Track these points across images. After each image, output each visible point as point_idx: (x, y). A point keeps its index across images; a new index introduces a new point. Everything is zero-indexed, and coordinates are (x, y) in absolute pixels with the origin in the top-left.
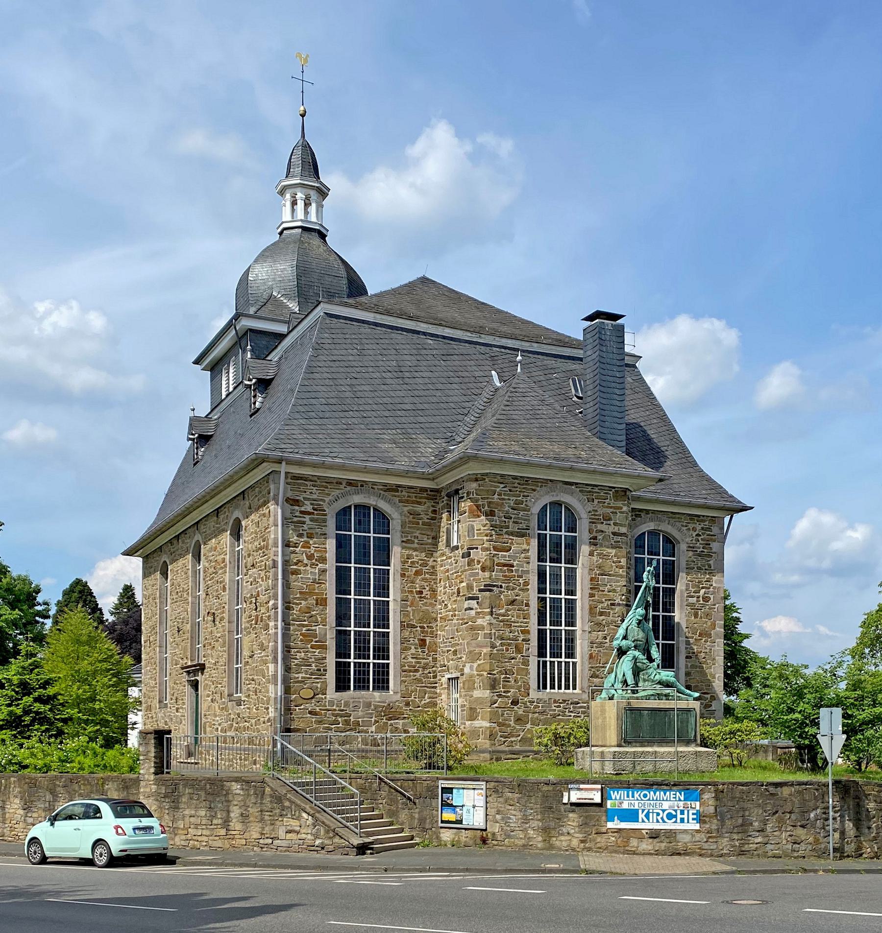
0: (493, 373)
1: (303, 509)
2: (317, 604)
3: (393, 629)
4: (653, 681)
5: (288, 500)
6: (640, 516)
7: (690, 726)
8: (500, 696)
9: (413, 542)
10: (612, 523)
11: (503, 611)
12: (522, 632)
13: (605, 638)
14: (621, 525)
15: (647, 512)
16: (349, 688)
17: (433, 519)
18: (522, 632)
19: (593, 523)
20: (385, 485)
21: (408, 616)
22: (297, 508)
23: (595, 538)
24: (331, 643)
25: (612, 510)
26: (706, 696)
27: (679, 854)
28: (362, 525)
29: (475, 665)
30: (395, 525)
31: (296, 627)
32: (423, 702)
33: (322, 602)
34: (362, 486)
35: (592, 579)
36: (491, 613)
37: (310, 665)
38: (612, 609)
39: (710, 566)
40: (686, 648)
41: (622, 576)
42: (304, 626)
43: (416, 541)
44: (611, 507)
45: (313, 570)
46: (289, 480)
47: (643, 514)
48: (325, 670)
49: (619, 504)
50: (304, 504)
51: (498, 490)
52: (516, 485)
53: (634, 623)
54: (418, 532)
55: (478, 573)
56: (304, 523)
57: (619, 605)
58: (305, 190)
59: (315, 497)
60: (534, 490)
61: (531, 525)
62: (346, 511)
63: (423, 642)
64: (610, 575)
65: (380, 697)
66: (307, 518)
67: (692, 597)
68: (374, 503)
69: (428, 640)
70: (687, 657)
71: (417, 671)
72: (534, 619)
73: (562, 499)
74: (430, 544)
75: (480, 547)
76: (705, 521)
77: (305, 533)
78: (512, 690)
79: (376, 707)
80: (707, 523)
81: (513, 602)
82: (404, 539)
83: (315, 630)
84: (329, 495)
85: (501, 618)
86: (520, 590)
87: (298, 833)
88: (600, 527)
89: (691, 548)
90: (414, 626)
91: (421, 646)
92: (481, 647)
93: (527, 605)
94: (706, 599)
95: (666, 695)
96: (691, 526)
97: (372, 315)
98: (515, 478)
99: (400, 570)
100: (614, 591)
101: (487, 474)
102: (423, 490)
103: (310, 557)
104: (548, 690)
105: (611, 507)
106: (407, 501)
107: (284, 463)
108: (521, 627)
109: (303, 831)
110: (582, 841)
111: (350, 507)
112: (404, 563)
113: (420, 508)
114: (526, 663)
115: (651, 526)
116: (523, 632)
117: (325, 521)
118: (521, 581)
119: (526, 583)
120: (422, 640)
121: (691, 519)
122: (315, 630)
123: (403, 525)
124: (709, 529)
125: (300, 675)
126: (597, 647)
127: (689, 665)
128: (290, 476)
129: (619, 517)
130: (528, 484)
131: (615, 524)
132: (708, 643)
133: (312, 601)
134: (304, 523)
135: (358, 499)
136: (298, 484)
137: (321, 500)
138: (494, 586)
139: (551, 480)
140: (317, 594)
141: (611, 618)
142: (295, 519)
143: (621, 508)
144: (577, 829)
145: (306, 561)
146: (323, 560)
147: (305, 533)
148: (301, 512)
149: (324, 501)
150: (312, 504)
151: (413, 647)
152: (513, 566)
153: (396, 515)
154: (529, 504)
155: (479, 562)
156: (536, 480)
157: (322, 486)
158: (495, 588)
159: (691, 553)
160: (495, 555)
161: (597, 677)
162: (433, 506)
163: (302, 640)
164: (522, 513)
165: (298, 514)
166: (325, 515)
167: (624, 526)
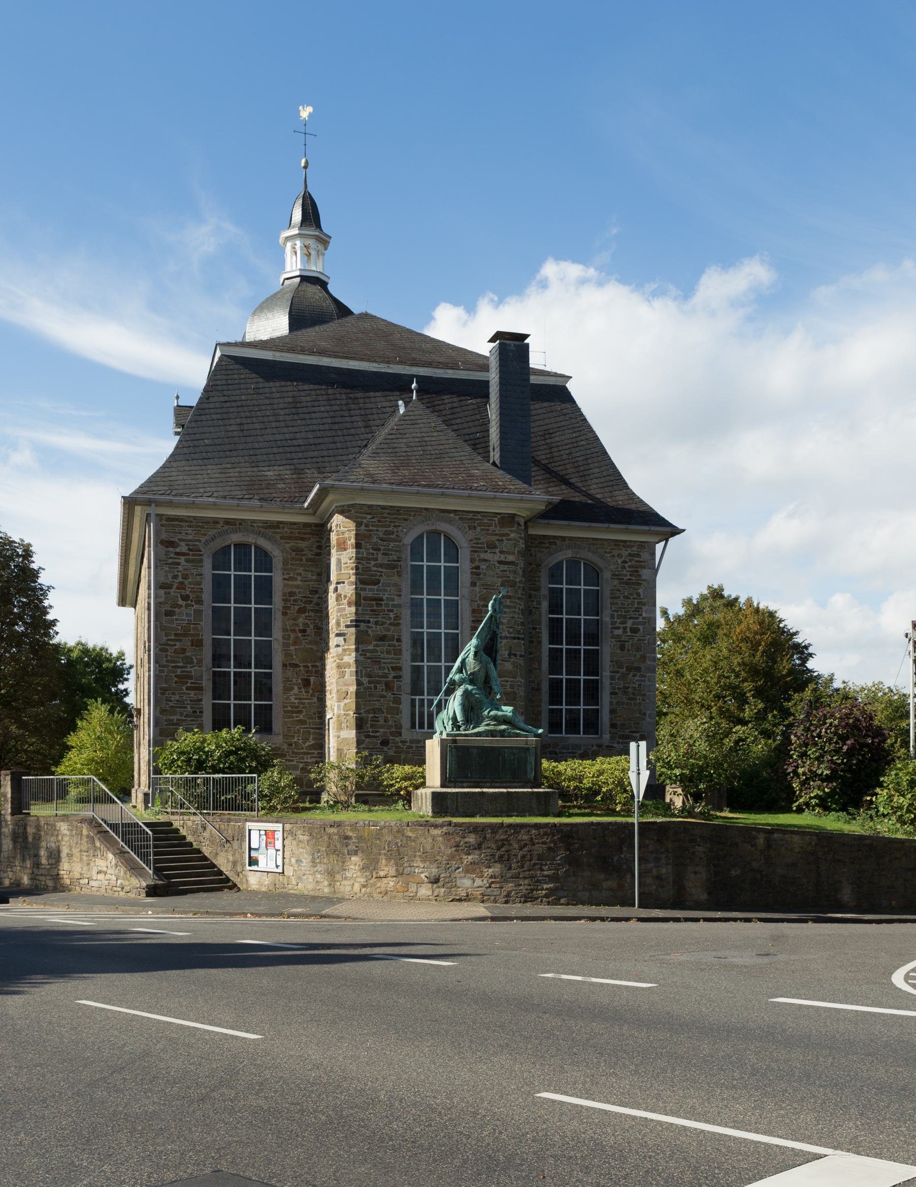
0: (400, 402)
1: (178, 550)
2: (192, 645)
3: (277, 671)
5: (162, 542)
6: (555, 543)
7: (529, 767)
8: (368, 736)
9: (296, 579)
10: (497, 551)
11: (371, 647)
12: (393, 668)
14: (508, 553)
15: (563, 539)
17: (318, 554)
18: (393, 668)
19: (475, 552)
20: (266, 522)
22: (171, 549)
23: (478, 568)
25: (496, 537)
26: (635, 735)
27: (460, 900)
28: (243, 564)
29: (342, 704)
30: (277, 563)
32: (307, 744)
33: (198, 643)
34: (240, 524)
35: (474, 611)
39: (639, 594)
40: (611, 684)
43: (299, 578)
44: (497, 535)
46: (164, 522)
47: (558, 542)
48: (201, 712)
49: (506, 530)
50: (178, 545)
51: (365, 521)
52: (385, 515)
53: (472, 653)
54: (302, 569)
55: (344, 609)
56: (179, 564)
57: (506, 638)
58: (304, 240)
59: (190, 537)
60: (406, 520)
62: (225, 550)
63: (306, 683)
67: (618, 628)
68: (254, 541)
69: (312, 679)
70: (612, 693)
71: (300, 712)
72: (407, 654)
73: (439, 528)
74: (314, 581)
75: (346, 581)
76: (632, 547)
77: (180, 574)
78: (382, 730)
80: (635, 549)
81: (382, 638)
82: (286, 577)
83: (191, 672)
85: (368, 655)
86: (391, 624)
87: (106, 873)
88: (483, 556)
89: (614, 576)
90: (296, 666)
91: (305, 686)
92: (347, 685)
93: (399, 640)
94: (634, 630)
96: (616, 552)
97: (271, 353)
98: (384, 508)
99: (281, 608)
101: (352, 505)
102: (306, 525)
103: (185, 598)
104: (426, 729)
105: (497, 535)
106: (289, 538)
107: (153, 505)
108: (391, 663)
109: (109, 872)
110: (364, 886)
111: (229, 546)
112: (285, 600)
113: (302, 544)
114: (398, 701)
115: (569, 554)
116: (393, 669)
117: (201, 561)
118: (392, 615)
119: (397, 617)
120: (306, 680)
121: (615, 545)
123: (285, 562)
124: (638, 555)
127: (615, 701)
128: (164, 518)
129: (506, 545)
130: (400, 514)
131: (502, 552)
132: (637, 678)
133: (187, 641)
134: (179, 564)
135: (236, 538)
136: (173, 526)
137: (197, 540)
139: (426, 509)
142: (170, 561)
143: (509, 535)
144: (359, 873)
145: (181, 602)
146: (199, 601)
147: (180, 574)
148: (176, 553)
149: (200, 541)
150: (187, 545)
151: (296, 688)
152: (382, 600)
153: (277, 554)
154: (400, 534)
155: (345, 597)
156: (408, 510)
157: (198, 526)
159: (616, 582)
162: (318, 542)
163: (176, 682)
164: (392, 544)
165: (172, 555)
166: (202, 555)
167: (513, 554)
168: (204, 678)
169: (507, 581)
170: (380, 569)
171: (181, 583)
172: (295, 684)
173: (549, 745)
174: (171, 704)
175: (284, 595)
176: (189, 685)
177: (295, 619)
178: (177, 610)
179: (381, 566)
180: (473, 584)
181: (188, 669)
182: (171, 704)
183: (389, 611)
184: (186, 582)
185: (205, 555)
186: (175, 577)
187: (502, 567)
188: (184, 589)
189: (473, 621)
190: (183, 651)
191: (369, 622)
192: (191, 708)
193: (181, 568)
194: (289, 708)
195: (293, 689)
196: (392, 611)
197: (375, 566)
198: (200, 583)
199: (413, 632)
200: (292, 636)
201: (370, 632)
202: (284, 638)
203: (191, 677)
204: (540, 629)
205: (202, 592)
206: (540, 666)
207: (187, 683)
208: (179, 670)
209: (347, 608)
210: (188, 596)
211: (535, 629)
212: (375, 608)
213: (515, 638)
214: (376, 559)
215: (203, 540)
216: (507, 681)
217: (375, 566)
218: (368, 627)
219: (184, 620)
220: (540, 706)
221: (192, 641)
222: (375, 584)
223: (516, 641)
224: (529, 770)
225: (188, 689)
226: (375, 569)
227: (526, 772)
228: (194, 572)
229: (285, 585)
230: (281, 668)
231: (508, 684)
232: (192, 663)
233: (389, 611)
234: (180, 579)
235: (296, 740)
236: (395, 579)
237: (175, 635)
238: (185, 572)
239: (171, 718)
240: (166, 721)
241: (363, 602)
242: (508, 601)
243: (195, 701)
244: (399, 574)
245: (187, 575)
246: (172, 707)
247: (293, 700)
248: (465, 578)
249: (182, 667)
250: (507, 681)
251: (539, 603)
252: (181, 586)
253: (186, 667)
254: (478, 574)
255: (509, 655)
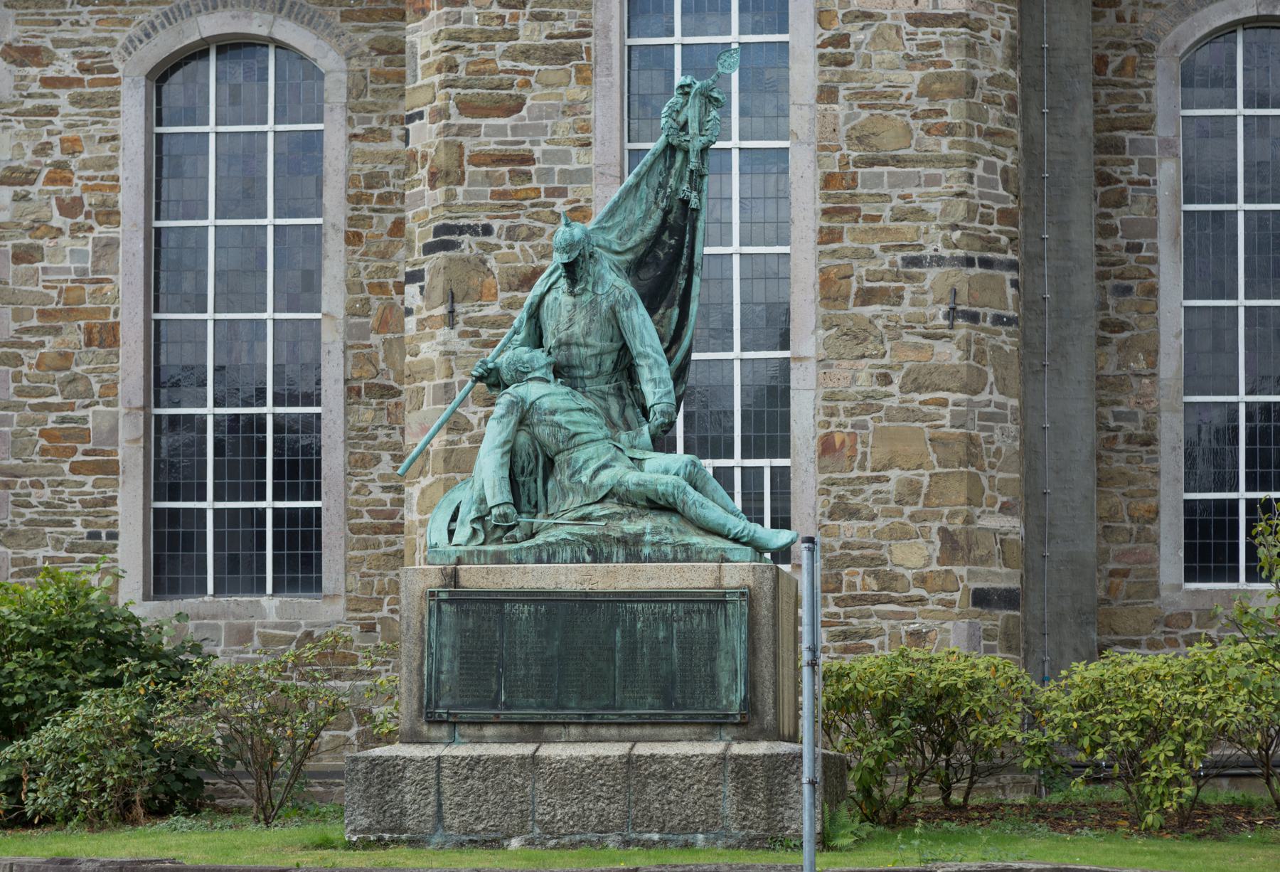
1: (50, 72)
2: (89, 343)
4: (587, 491)
7: (723, 664)
9: (387, 136)
11: (493, 310)
13: (885, 379)
16: (203, 591)
21: (371, 360)
22: (33, 71)
24: (131, 454)
30: (335, 91)
31: (28, 411)
33: (104, 336)
35: (828, 181)
36: (451, 319)
37: (69, 523)
38: (910, 278)
41: (947, 162)
42: (48, 407)
45: (78, 245)
48: (113, 536)
56: (53, 111)
57: (939, 261)
59: (86, 34)
61: (598, 18)
64: (898, 161)
65: (280, 610)
66: (63, 98)
77: (55, 140)
79: (267, 641)
82: (359, 130)
83: (84, 420)
84: (126, 22)
95: (623, 541)
99: (342, 223)
100: (920, 214)
103: (70, 208)
112: (355, 200)
117: (114, 99)
122: (84, 420)
123: (356, 91)
125: (40, 553)
126: (850, 413)
133: (73, 335)
134: (53, 111)
138: (461, 230)
140: (89, 313)
141: (906, 308)
142: (29, 104)
145: (58, 220)
146: (109, 214)
147: (55, 140)
148: (46, 82)
150: (75, 54)
152: (528, 159)
158: (466, 238)
160: (462, 130)
161: (853, 514)
163: (44, 451)
166: (116, 82)
168: (122, 436)
169: (939, 77)
170: (524, 66)
171: (59, 166)
172: (382, 447)
173: (1187, 615)
174: (28, 514)
175: (352, 181)
176: (79, 457)
177: (383, 255)
178: (46, 242)
179: (526, 53)
180: (827, 94)
181: (79, 413)
182: (28, 514)
183: (552, 192)
184: (74, 163)
185: (126, 82)
186: (44, 149)
187: (923, 34)
188: (68, 181)
189: (825, 212)
190: (65, 359)
191: (487, 230)
192: (86, 524)
193: (58, 122)
194: (366, 519)
195: (378, 460)
196: (561, 193)
197: (507, 54)
198: (110, 163)
199: (319, 216)
200: (376, 303)
201: (492, 263)
202: (351, 313)
203: (84, 436)
204: (1154, 248)
205: (115, 188)
206: (1153, 364)
207: (75, 451)
208: (53, 416)
209: (428, 192)
210: (78, 202)
211: (1136, 248)
212: (508, 186)
213: (969, 262)
214: (512, 35)
215: (121, 38)
216: (943, 403)
217: (507, 54)
218: (487, 248)
219: (68, 271)
220: (1155, 493)
221: (89, 331)
222: (509, 112)
223: (977, 270)
224: (724, 679)
225: (75, 469)
226: (509, 64)
227: (713, 683)
228: (97, 130)
229: (352, 158)
230: (341, 400)
231: (946, 412)
232: (88, 393)
233: (552, 192)
234: (57, 155)
235: (385, 612)
236: (574, 91)
237: (43, 314)
238: (70, 134)
239: (29, 554)
240: (14, 563)
241: (469, 169)
242: (945, 142)
243: (95, 504)
244: (585, 78)
245: (76, 141)
246: (30, 522)
247: (378, 494)
248: (804, 74)
249: (59, 407)
250: (943, 403)
251: (1149, 167)
252: (60, 174)
253: (72, 407)
254: (843, 62)
255: (952, 314)
